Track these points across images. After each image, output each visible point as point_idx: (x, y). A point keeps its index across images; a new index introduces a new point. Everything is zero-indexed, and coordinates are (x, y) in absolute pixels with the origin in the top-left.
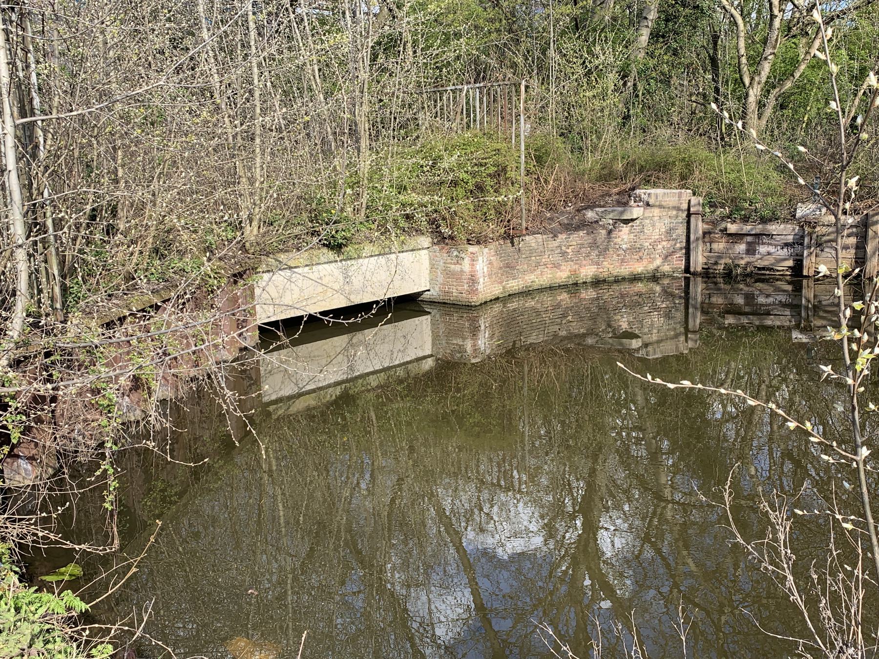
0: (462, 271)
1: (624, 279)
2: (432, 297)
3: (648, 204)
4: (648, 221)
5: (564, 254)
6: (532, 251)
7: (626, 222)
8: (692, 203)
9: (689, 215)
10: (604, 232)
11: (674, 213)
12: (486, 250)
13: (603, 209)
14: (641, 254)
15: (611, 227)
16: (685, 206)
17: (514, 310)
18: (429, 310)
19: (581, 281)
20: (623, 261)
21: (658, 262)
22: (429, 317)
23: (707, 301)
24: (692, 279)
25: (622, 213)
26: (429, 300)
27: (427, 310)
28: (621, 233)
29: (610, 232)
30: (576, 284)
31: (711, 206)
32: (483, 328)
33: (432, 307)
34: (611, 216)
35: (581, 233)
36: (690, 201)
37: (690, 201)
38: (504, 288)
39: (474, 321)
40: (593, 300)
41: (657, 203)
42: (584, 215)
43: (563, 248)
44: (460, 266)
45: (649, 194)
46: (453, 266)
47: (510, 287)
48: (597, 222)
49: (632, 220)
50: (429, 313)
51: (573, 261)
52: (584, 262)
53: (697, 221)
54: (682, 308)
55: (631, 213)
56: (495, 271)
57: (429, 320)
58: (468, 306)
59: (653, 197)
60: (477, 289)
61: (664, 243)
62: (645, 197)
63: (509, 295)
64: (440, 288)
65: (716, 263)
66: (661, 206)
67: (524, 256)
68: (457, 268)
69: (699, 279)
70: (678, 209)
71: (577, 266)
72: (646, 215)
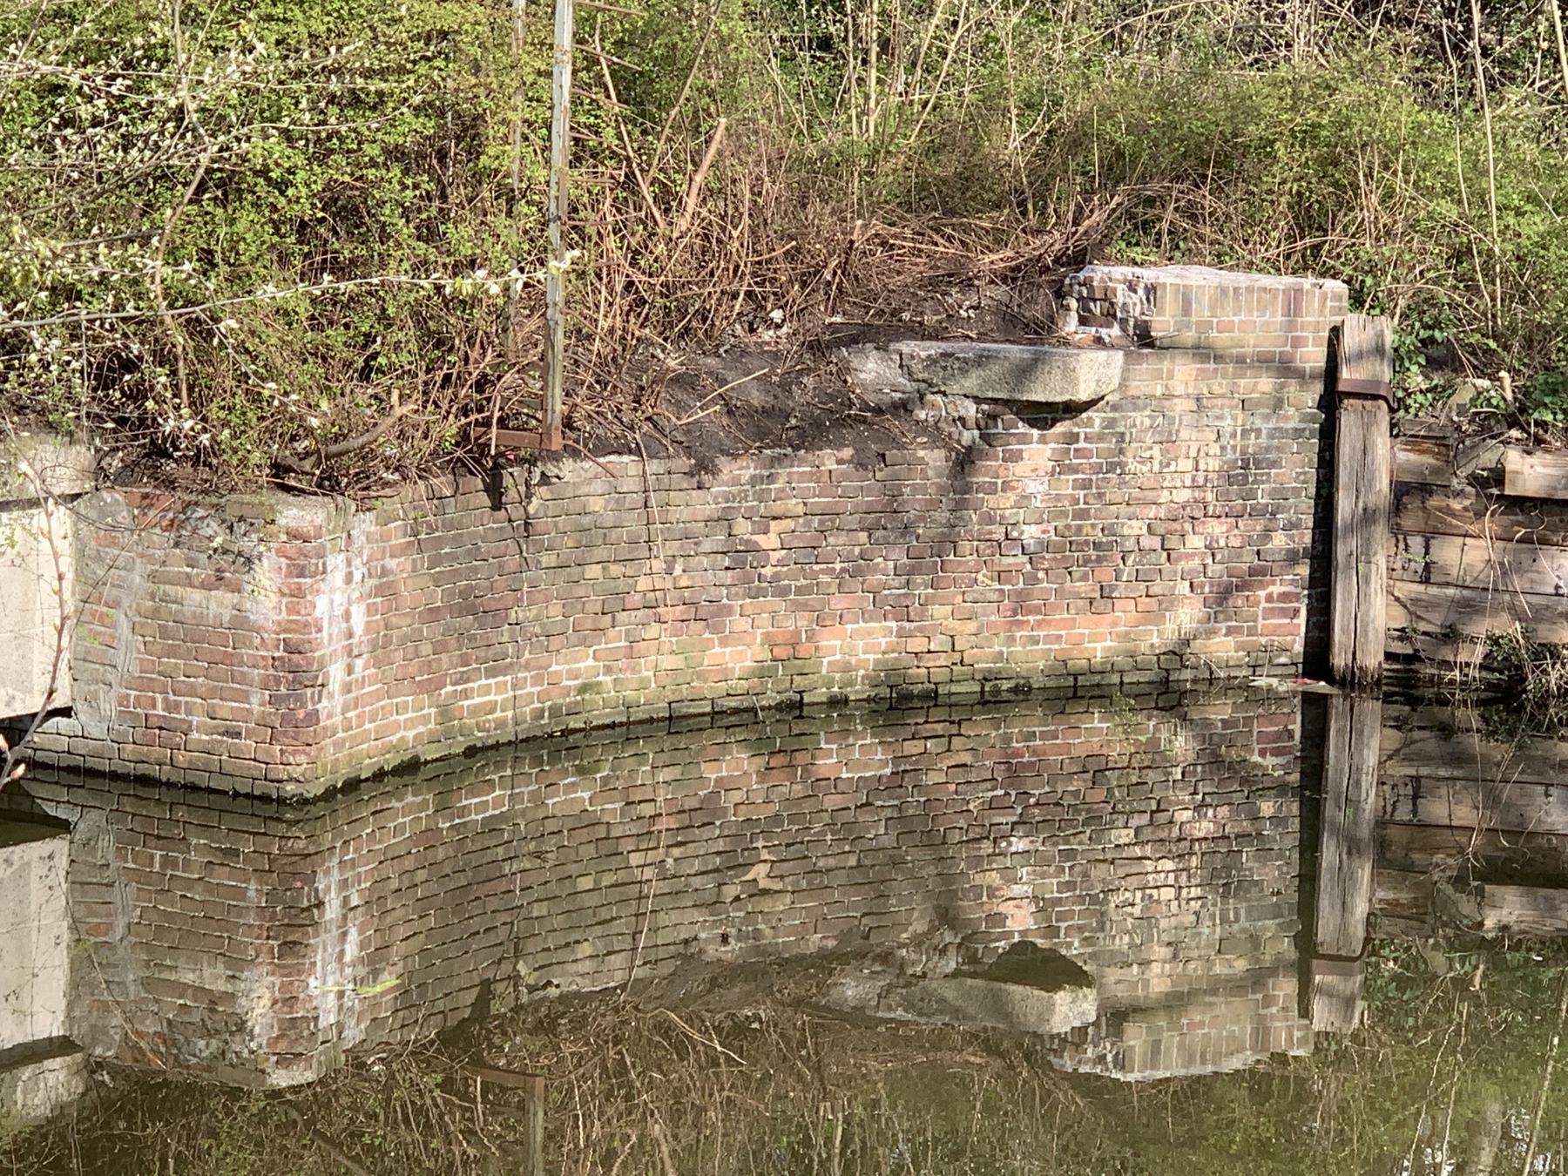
0: (241, 622)
1: (1023, 691)
2: (81, 746)
3: (1144, 338)
4: (1142, 418)
5: (741, 556)
6: (589, 535)
7: (1044, 415)
8: (1349, 342)
9: (1331, 401)
10: (935, 459)
11: (1266, 384)
12: (365, 524)
13: (933, 348)
14: (1105, 574)
15: (969, 436)
16: (1314, 356)
17: (491, 827)
18: (61, 813)
19: (821, 695)
20: (1021, 604)
21: (1187, 615)
22: (59, 847)
23: (1403, 813)
24: (1338, 704)
25: (1025, 372)
26: (66, 761)
27: (50, 809)
28: (1018, 469)
29: (964, 461)
30: (795, 708)
31: (1433, 364)
32: (332, 911)
33: (80, 796)
34: (971, 382)
35: (829, 459)
36: (1336, 332)
37: (1336, 332)
38: (445, 713)
39: (299, 869)
40: (876, 786)
41: (1189, 336)
42: (844, 370)
43: (742, 527)
44: (230, 598)
45: (1151, 290)
46: (197, 595)
47: (474, 711)
48: (902, 407)
49: (1072, 409)
50: (62, 827)
51: (783, 592)
52: (839, 602)
53: (1367, 427)
54: (1288, 839)
55: (1069, 373)
56: (404, 625)
57: (62, 862)
58: (265, 799)
59: (1169, 303)
60: (313, 717)
61: (1217, 528)
62: (1132, 303)
63: (471, 752)
64: (123, 701)
65: (1450, 636)
66: (1203, 352)
67: (548, 559)
68: (219, 604)
69: (1371, 708)
70: (1284, 368)
71: (803, 621)
72: (1138, 387)
